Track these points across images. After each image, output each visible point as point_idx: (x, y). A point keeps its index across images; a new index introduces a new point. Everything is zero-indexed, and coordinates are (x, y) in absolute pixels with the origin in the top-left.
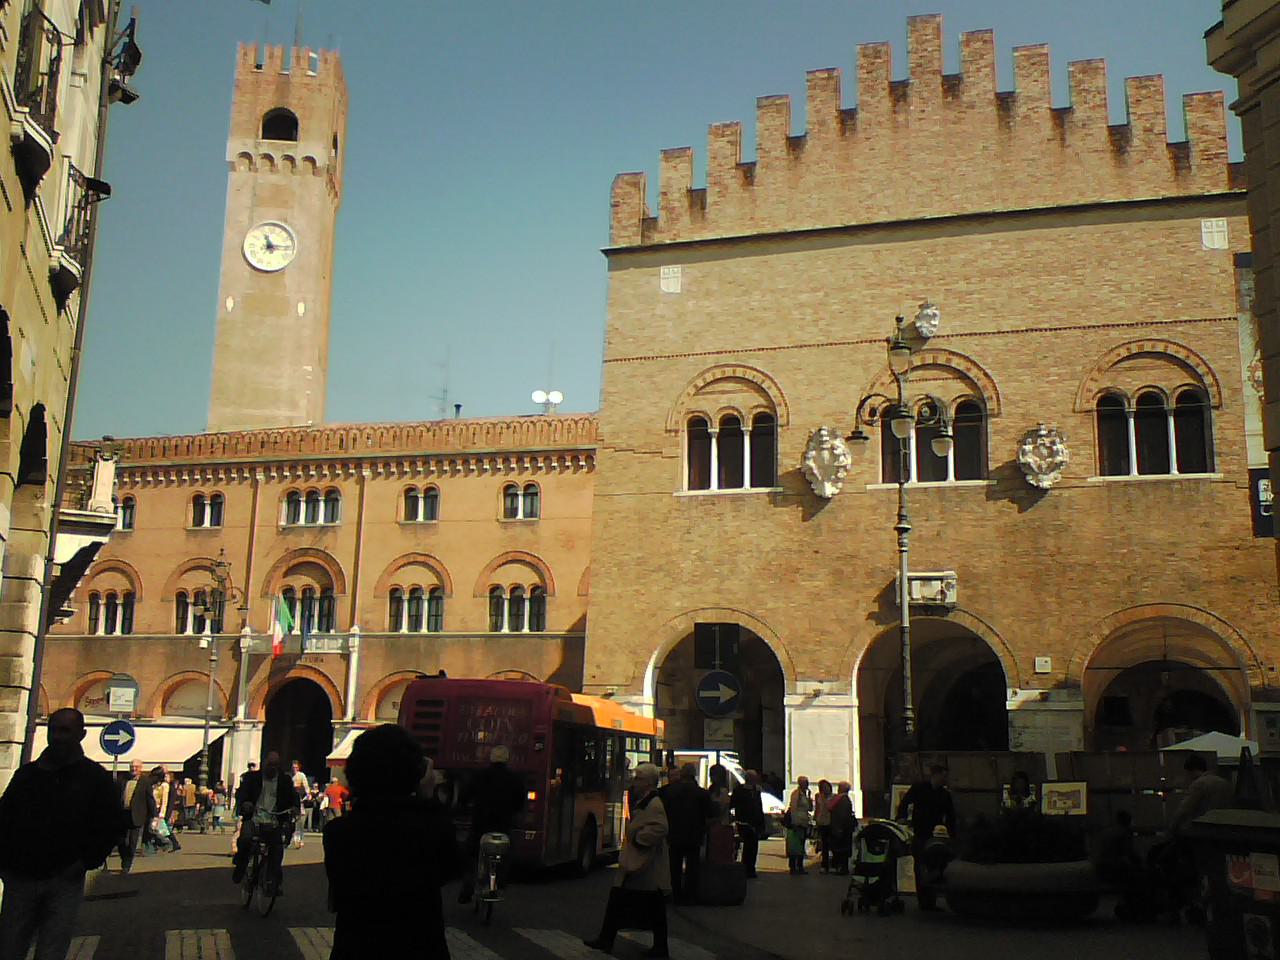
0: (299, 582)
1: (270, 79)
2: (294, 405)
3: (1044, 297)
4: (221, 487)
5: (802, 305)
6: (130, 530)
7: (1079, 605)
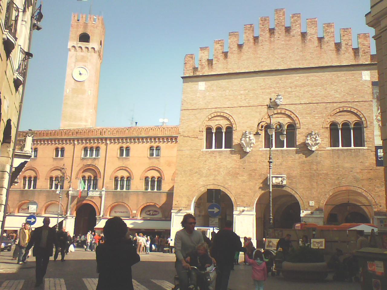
0: (87, 174)
2: (87, 121)
3: (314, 93)
5: (241, 94)
7: (323, 186)
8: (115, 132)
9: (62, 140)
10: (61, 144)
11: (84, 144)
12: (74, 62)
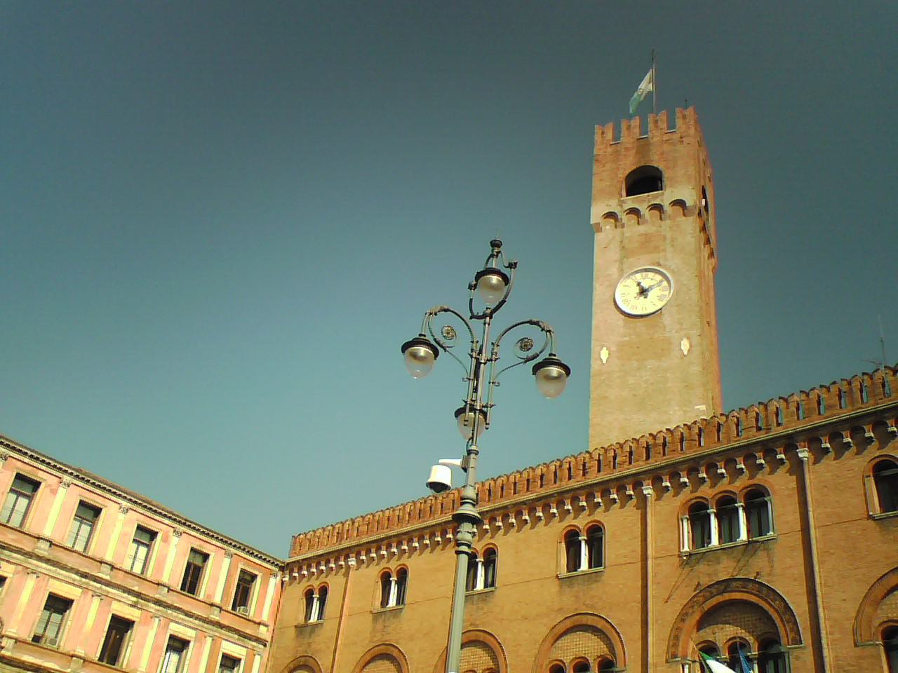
0: (723, 634)
1: (628, 145)
4: (599, 515)
6: (492, 589)
8: (830, 398)
9: (589, 491)
10: (586, 512)
11: (687, 490)
12: (616, 261)
